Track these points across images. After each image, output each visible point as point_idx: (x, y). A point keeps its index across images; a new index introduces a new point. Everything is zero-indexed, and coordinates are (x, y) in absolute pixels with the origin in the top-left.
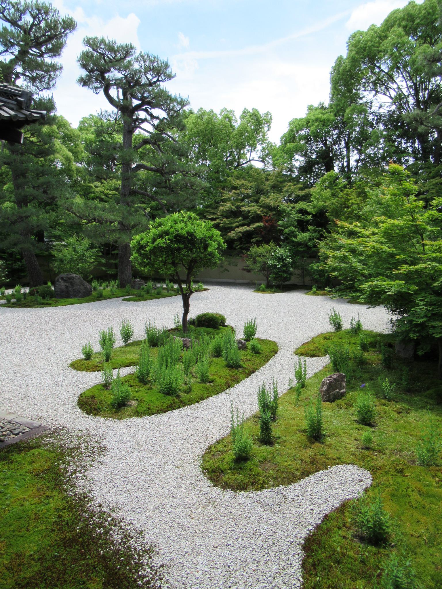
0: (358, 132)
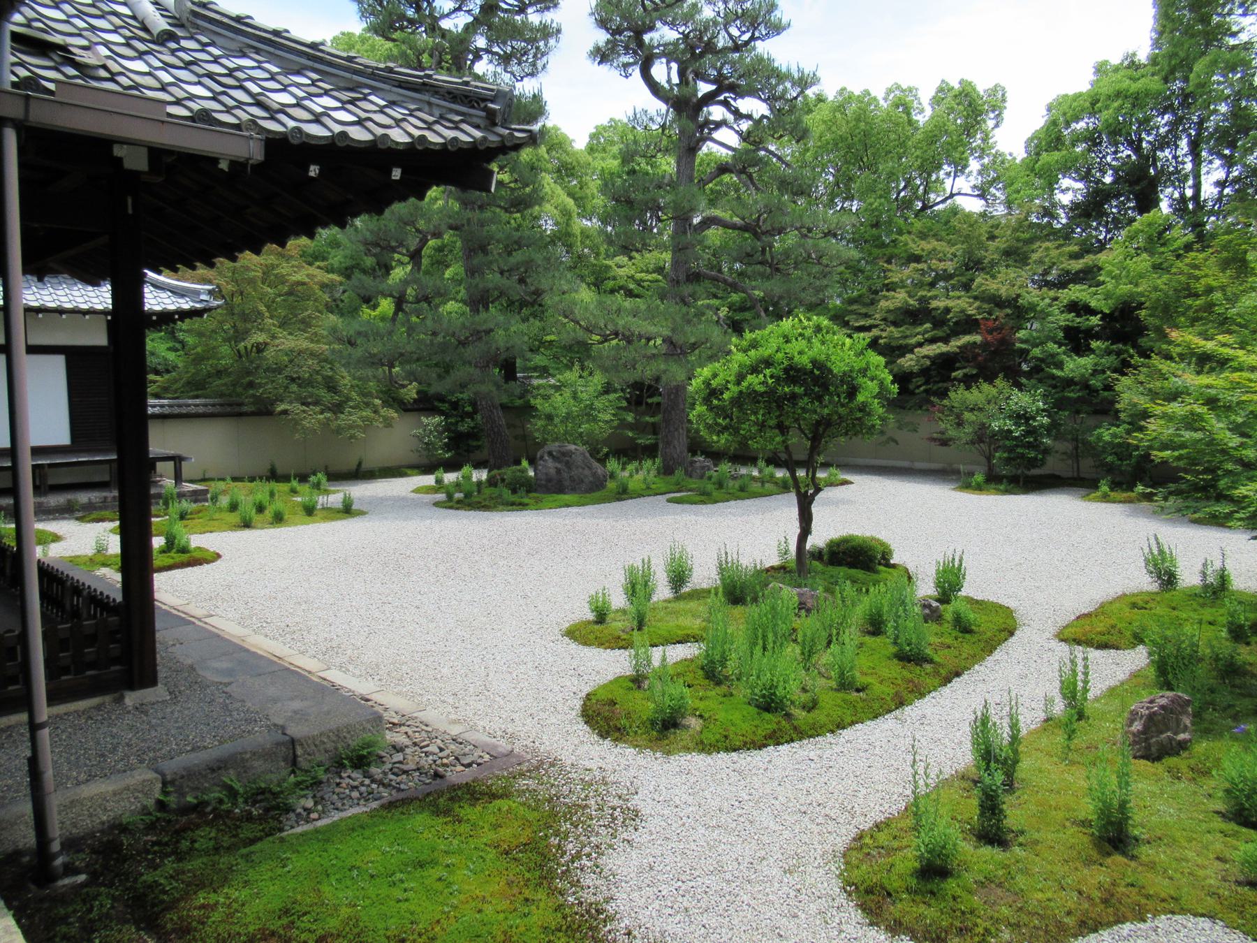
0: (1223, 115)
